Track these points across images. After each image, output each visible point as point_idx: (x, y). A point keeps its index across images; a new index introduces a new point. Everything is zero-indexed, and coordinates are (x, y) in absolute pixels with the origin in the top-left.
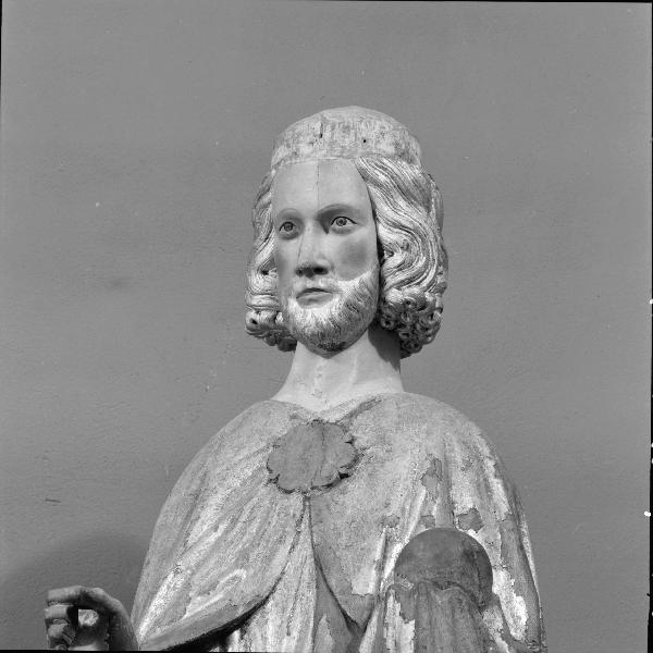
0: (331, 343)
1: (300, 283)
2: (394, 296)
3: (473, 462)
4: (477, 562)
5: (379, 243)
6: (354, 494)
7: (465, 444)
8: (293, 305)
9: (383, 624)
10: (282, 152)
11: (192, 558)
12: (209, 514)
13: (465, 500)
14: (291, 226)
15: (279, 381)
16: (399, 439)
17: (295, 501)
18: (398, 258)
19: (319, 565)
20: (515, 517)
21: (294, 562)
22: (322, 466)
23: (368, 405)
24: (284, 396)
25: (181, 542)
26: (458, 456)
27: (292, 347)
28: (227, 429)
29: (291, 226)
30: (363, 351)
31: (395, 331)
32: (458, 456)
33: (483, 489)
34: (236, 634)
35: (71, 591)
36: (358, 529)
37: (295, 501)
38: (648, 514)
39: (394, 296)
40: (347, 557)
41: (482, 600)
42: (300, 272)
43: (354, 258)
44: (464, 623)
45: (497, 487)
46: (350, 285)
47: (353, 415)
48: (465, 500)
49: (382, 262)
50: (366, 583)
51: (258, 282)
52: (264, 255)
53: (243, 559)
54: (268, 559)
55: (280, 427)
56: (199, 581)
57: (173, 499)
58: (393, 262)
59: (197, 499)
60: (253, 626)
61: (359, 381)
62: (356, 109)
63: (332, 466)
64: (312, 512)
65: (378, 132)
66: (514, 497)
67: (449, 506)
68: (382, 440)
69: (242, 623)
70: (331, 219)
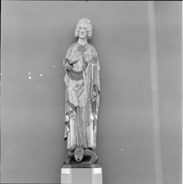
1: (81, 33)
2: (89, 35)
3: (94, 50)
4: (96, 59)
5: (88, 31)
7: (94, 49)
11: (71, 56)
13: (94, 54)
16: (89, 48)
17: (81, 52)
18: (89, 32)
22: (82, 49)
34: (81, 160)
37: (81, 52)
38: (1, 85)
43: (86, 31)
48: (94, 54)
63: (84, 50)
64: (82, 54)
68: (88, 48)
69: (76, 62)
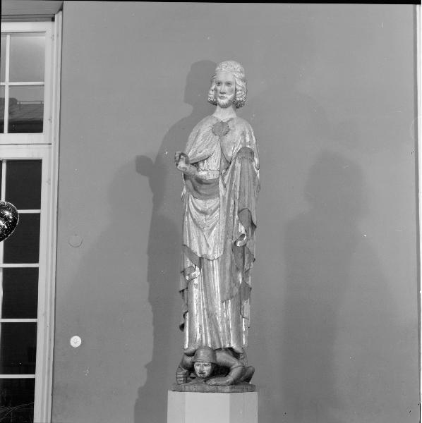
0: (225, 106)
1: (220, 95)
3: (250, 133)
4: (252, 153)
6: (228, 137)
8: (219, 99)
9: (235, 163)
10: (218, 68)
12: (200, 137)
14: (219, 83)
15: (213, 112)
17: (217, 137)
19: (222, 150)
20: (256, 143)
21: (217, 149)
22: (221, 130)
23: (231, 119)
24: (215, 115)
25: (194, 142)
26: (247, 131)
27: (216, 105)
28: (204, 120)
29: (219, 83)
30: (231, 108)
31: (236, 105)
32: (247, 131)
33: (251, 138)
35: (180, 152)
36: (229, 144)
39: (238, 99)
40: (227, 149)
41: (252, 160)
42: (221, 93)
44: (250, 165)
45: (254, 137)
46: (229, 97)
47: (228, 121)
48: (248, 139)
49: (236, 92)
50: (230, 155)
51: (211, 92)
52: (213, 88)
53: (207, 147)
54: (212, 147)
55: (215, 122)
56: (199, 150)
57: (192, 133)
58: (238, 93)
59: (198, 134)
60: (209, 160)
61: (229, 114)
62: (234, 62)
65: (238, 67)
66: (256, 140)
67: (245, 140)
68: (233, 127)
70: (228, 84)
